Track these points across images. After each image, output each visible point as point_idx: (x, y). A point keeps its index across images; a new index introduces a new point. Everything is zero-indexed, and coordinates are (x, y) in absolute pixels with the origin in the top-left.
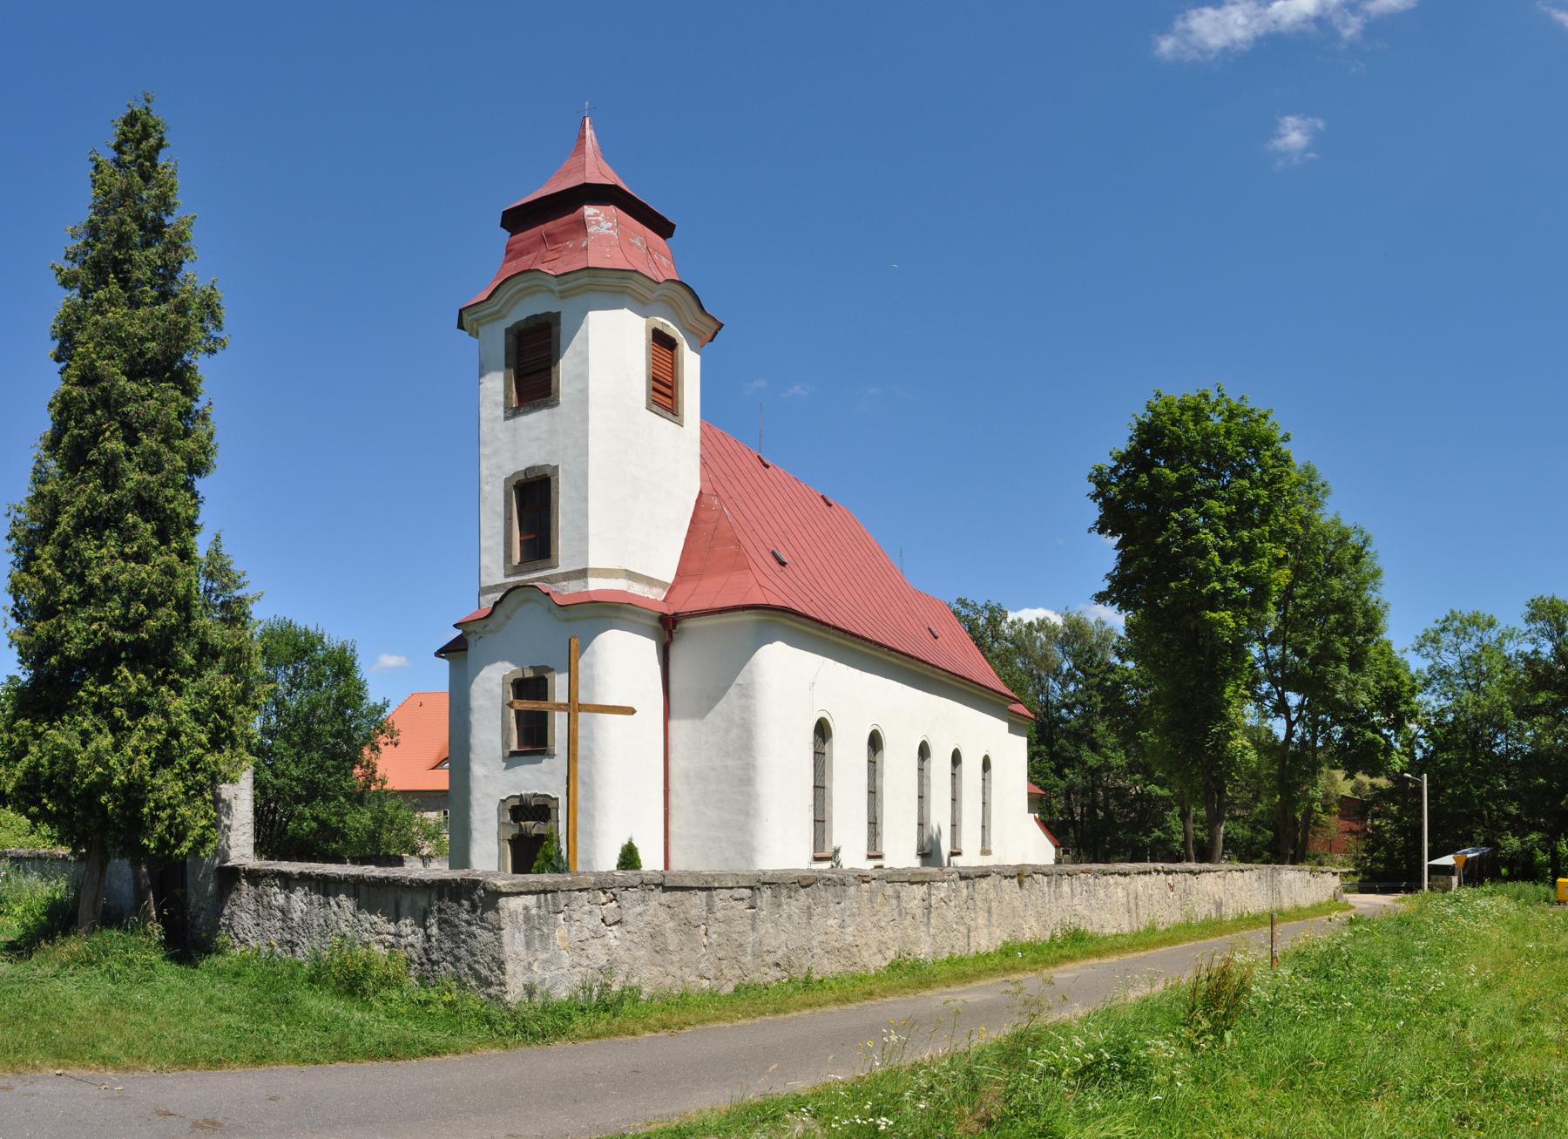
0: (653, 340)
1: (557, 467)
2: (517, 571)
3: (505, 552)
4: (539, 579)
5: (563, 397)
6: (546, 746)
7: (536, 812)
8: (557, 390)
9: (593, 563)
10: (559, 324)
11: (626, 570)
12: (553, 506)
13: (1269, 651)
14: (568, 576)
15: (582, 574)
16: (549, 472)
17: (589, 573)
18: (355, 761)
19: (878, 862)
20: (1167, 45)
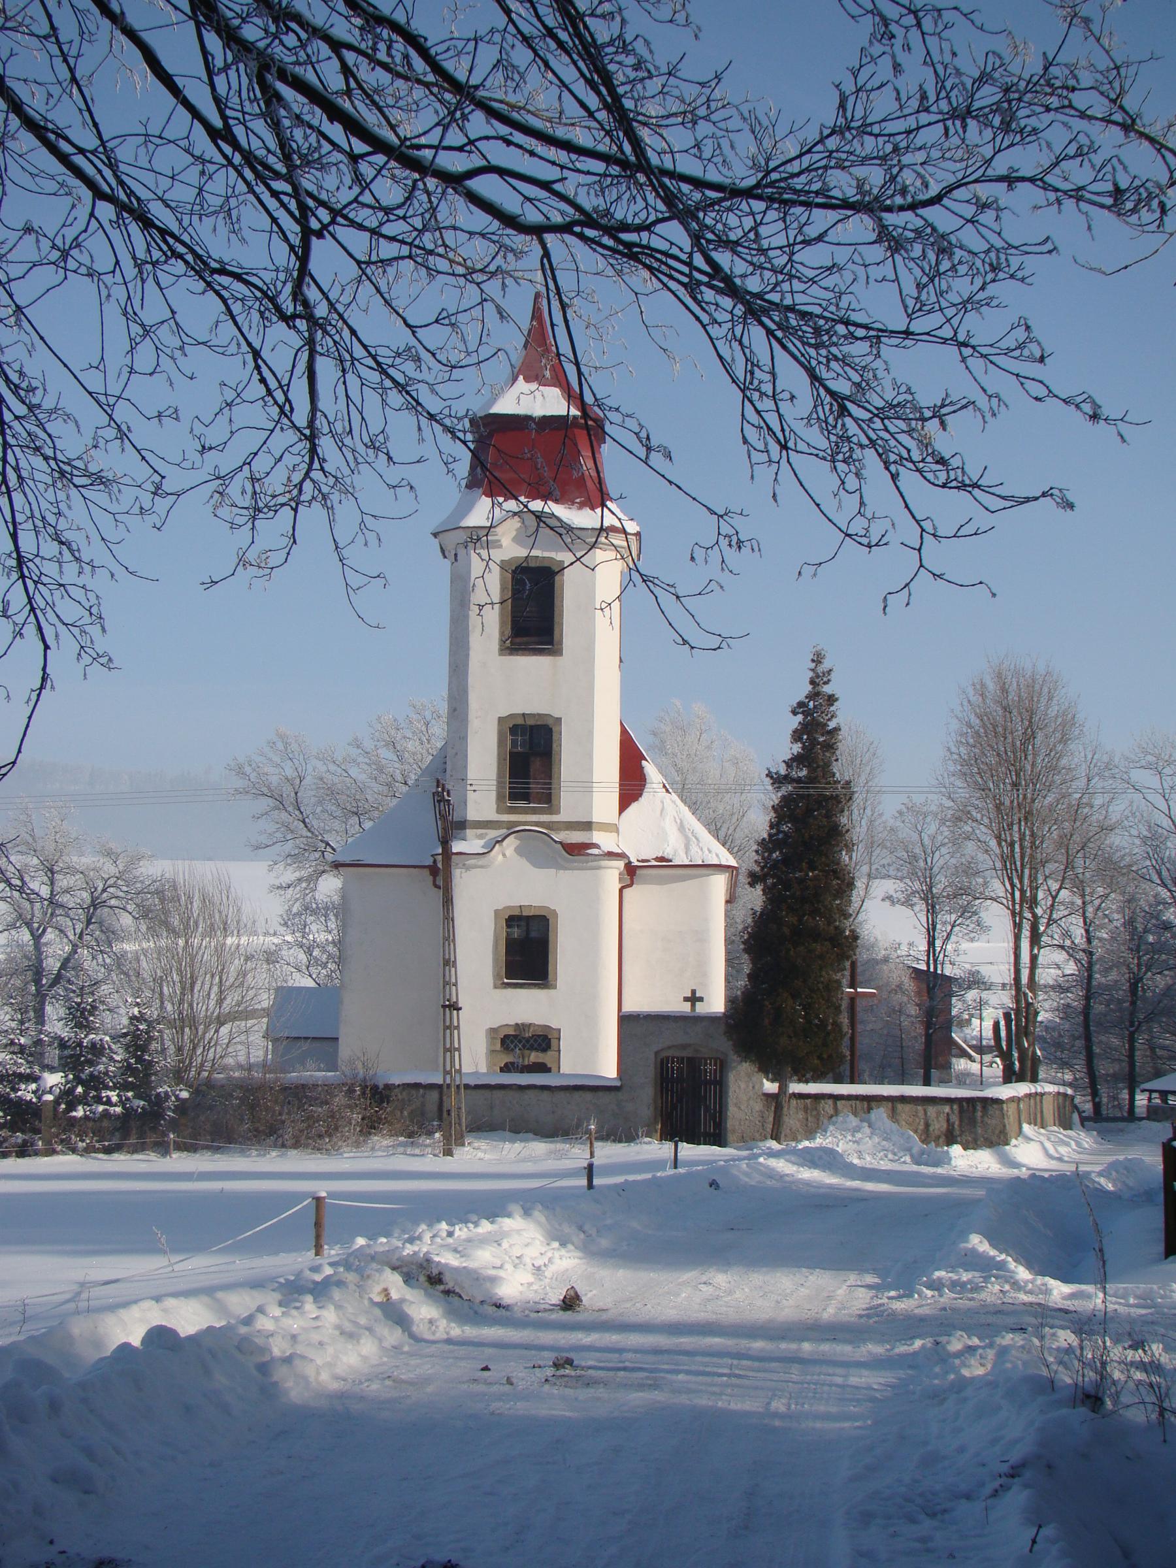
1: (560, 719)
16: (550, 722)
17: (594, 826)
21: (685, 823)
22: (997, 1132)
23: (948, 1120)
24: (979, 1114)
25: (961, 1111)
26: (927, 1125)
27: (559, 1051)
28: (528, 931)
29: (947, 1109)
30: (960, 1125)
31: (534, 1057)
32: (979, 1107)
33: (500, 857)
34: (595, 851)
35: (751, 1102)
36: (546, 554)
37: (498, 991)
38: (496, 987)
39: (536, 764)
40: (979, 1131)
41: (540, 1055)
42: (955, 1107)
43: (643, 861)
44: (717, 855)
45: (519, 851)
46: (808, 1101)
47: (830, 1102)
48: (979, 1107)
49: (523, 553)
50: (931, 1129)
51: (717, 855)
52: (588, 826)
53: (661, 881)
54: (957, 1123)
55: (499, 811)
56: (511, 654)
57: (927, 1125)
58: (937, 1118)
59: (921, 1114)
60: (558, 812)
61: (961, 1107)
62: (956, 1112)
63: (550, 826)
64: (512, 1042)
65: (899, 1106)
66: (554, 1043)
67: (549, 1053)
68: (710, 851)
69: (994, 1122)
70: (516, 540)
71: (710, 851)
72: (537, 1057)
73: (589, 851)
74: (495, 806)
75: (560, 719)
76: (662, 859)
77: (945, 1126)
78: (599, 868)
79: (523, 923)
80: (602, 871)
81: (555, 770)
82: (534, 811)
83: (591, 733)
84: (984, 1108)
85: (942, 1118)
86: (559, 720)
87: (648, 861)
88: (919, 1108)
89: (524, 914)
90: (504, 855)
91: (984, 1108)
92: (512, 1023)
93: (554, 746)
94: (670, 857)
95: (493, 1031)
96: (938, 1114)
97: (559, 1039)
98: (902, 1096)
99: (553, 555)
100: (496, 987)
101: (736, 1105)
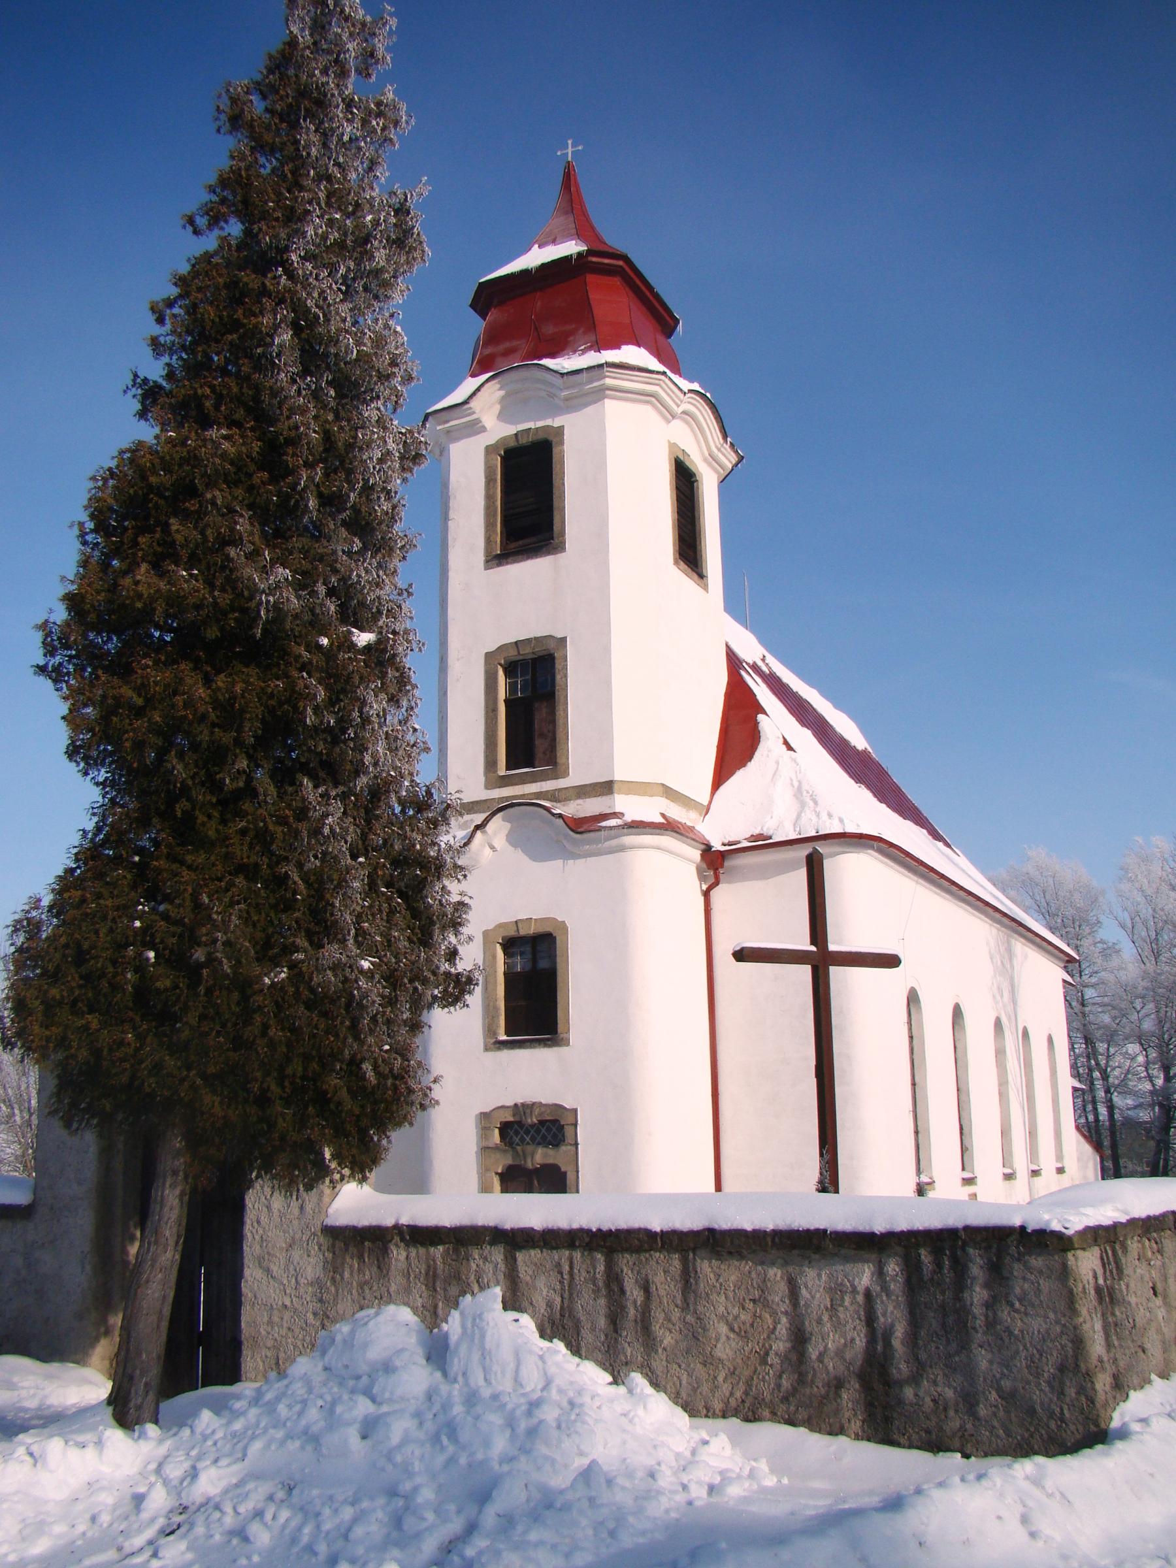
0: (680, 554)
1: (564, 640)
2: (505, 782)
3: (486, 757)
4: (539, 795)
5: (574, 1035)
6: (556, 1032)
7: (538, 1131)
8: (562, 533)
9: (620, 774)
10: (562, 443)
11: (663, 785)
12: (556, 482)
13: (1111, 1049)
14: (584, 791)
15: (606, 788)
16: (552, 645)
17: (616, 787)
18: (20, 950)
19: (971, 1189)
20: (785, 1481)
21: (805, 787)
22: (1049, 1369)
23: (870, 1319)
24: (978, 1295)
25: (914, 1282)
26: (799, 1338)
27: (576, 1144)
28: (534, 961)
29: (865, 1276)
30: (913, 1338)
31: (540, 1156)
32: (977, 1269)
33: (487, 851)
34: (612, 822)
35: (296, 1254)
36: (540, 424)
37: (490, 1054)
38: (486, 1049)
39: (540, 713)
40: (983, 1360)
41: (550, 1151)
42: (893, 1267)
43: (730, 844)
44: (841, 820)
45: (513, 840)
46: (438, 1251)
47: (497, 1254)
48: (977, 1269)
49: (510, 430)
50: (813, 1352)
51: (841, 820)
52: (606, 788)
53: (763, 873)
54: (900, 1331)
55: (489, 785)
56: (499, 565)
57: (799, 1338)
58: (833, 1309)
59: (779, 1293)
60: (566, 774)
61: (912, 1268)
62: (897, 1287)
63: (554, 796)
64: (517, 1133)
65: (706, 1268)
66: (568, 1131)
67: (563, 1148)
68: (830, 815)
69: (1037, 1325)
70: (502, 417)
71: (830, 815)
72: (545, 1155)
73: (604, 824)
74: (482, 779)
75: (564, 640)
76: (760, 837)
77: (860, 1342)
78: (622, 849)
79: (528, 949)
80: (628, 855)
81: (560, 713)
82: (533, 778)
83: (607, 650)
84: (997, 1273)
85: (850, 1310)
86: (563, 640)
87: (739, 842)
88: (775, 1273)
89: (522, 932)
90: (492, 848)
91: (997, 1273)
92: (510, 1103)
93: (558, 677)
94: (770, 833)
95: (485, 1116)
96: (836, 1291)
97: (575, 1125)
98: (711, 1231)
99: (549, 422)
100: (486, 1049)
101: (260, 1261)
